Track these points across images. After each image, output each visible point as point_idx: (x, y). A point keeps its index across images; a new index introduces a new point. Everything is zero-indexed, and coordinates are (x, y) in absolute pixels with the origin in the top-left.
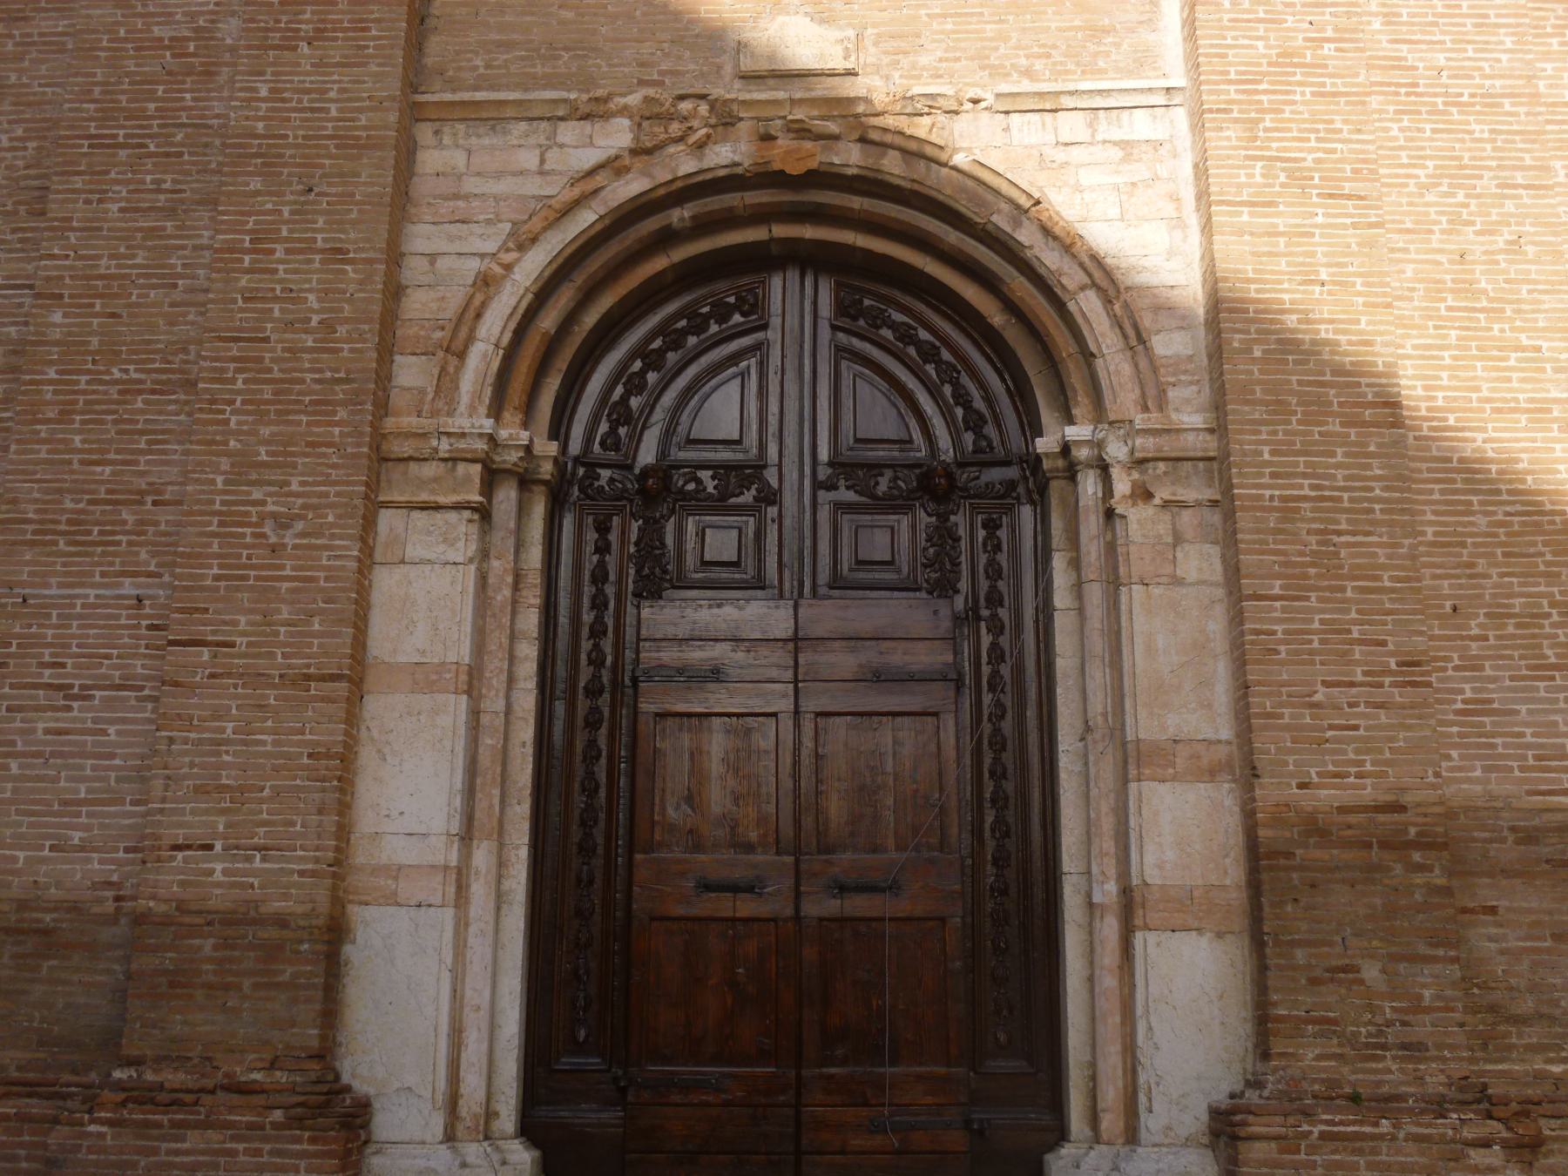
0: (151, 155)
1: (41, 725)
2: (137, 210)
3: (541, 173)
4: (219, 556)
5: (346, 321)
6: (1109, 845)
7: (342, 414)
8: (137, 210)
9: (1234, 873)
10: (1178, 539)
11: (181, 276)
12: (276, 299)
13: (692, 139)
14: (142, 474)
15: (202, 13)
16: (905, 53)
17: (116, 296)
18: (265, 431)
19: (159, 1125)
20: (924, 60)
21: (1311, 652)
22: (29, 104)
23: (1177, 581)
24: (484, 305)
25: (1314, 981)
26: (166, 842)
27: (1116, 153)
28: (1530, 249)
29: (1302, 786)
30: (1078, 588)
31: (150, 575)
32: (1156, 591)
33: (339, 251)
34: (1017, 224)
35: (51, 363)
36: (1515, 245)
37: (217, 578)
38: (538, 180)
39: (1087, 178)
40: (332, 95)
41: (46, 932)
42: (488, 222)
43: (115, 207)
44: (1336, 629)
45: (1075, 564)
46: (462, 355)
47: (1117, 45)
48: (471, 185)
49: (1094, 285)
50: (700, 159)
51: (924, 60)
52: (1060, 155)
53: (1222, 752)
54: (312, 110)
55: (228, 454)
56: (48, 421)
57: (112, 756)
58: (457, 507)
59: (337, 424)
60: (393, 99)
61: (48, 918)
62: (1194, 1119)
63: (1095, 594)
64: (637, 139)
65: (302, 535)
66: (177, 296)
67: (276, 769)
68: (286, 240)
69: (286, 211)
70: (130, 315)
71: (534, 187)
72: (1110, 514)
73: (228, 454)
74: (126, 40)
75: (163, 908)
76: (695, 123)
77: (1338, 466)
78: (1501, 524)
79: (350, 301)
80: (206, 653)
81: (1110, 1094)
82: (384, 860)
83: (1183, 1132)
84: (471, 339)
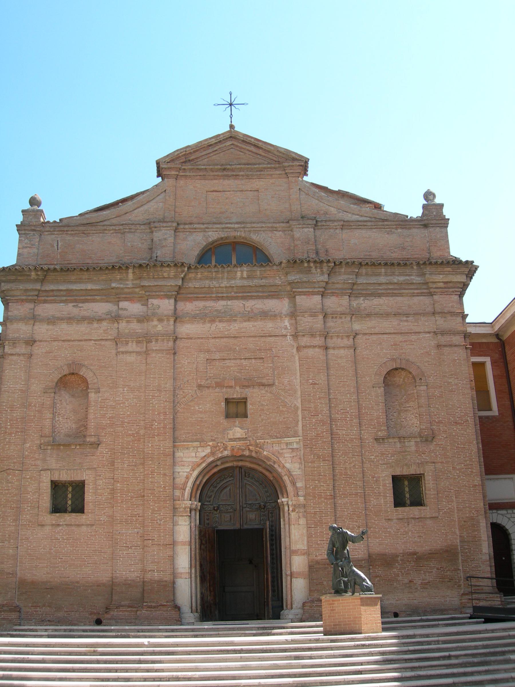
0: (131, 456)
1: (125, 553)
2: (130, 466)
3: (196, 457)
4: (151, 526)
5: (167, 486)
6: (289, 566)
7: (168, 502)
8: (130, 466)
9: (307, 569)
10: (299, 517)
11: (138, 477)
12: (156, 483)
13: (220, 450)
14: (136, 512)
15: (136, 429)
16: (256, 433)
17: (128, 481)
18: (156, 505)
19: (153, 610)
20: (259, 434)
21: (318, 536)
22: (108, 445)
23: (299, 524)
24: (188, 481)
25: (317, 585)
26: (147, 570)
27: (291, 450)
28: (357, 466)
29: (316, 556)
30: (284, 525)
31: (139, 528)
32: (296, 526)
33: (165, 474)
34: (274, 464)
35: (119, 493)
36: (354, 466)
37: (151, 529)
38: (195, 458)
39: (286, 455)
40: (161, 446)
41: (129, 584)
42: (188, 466)
43: (126, 465)
44: (321, 532)
45: (284, 520)
46: (185, 490)
47: (291, 430)
48: (184, 459)
49: (287, 475)
50: (222, 454)
51: (259, 434)
52: (281, 451)
53: (305, 551)
54: (159, 449)
55: (151, 509)
56: (119, 503)
57: (136, 557)
58: (186, 516)
59: (168, 504)
60: (171, 446)
61: (129, 582)
62: (300, 605)
63: (287, 526)
64: (211, 450)
65: (164, 522)
66: (138, 481)
67: (163, 559)
68: (156, 472)
69: (156, 467)
70: (131, 484)
71: (194, 460)
72: (289, 513)
73: (151, 509)
74: (124, 434)
75: (148, 580)
76: (221, 447)
77: (323, 506)
78: (349, 513)
79: (168, 483)
80: (151, 541)
81: (289, 602)
82: (179, 572)
83: (299, 607)
84: (186, 487)
